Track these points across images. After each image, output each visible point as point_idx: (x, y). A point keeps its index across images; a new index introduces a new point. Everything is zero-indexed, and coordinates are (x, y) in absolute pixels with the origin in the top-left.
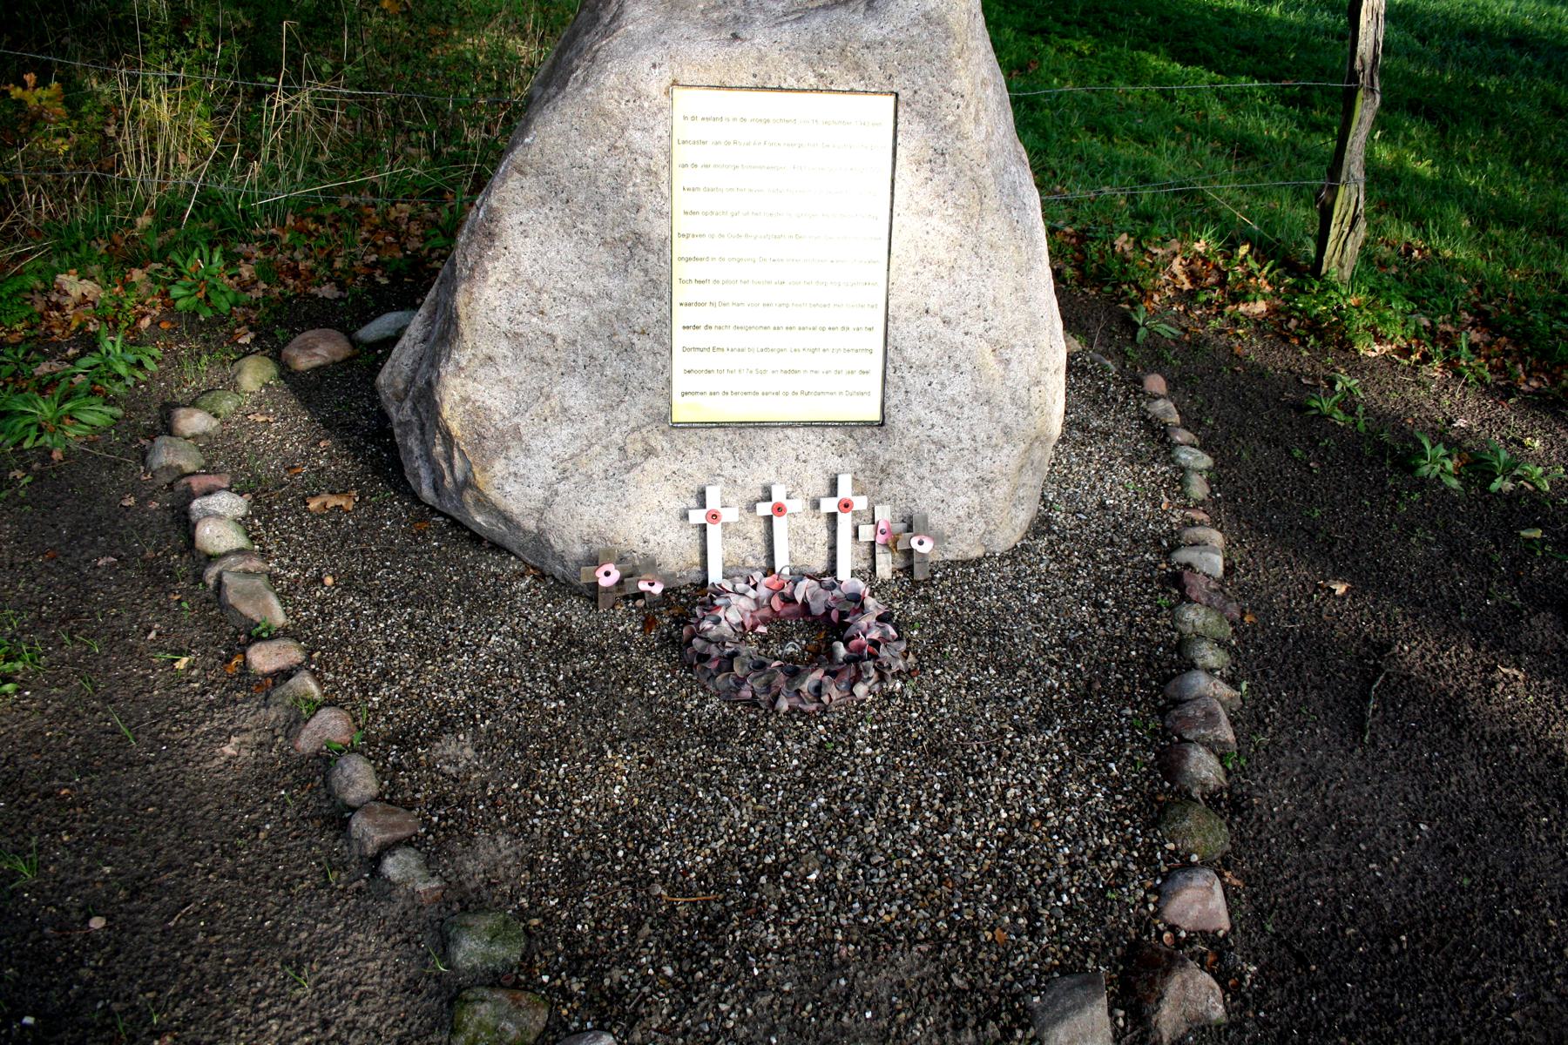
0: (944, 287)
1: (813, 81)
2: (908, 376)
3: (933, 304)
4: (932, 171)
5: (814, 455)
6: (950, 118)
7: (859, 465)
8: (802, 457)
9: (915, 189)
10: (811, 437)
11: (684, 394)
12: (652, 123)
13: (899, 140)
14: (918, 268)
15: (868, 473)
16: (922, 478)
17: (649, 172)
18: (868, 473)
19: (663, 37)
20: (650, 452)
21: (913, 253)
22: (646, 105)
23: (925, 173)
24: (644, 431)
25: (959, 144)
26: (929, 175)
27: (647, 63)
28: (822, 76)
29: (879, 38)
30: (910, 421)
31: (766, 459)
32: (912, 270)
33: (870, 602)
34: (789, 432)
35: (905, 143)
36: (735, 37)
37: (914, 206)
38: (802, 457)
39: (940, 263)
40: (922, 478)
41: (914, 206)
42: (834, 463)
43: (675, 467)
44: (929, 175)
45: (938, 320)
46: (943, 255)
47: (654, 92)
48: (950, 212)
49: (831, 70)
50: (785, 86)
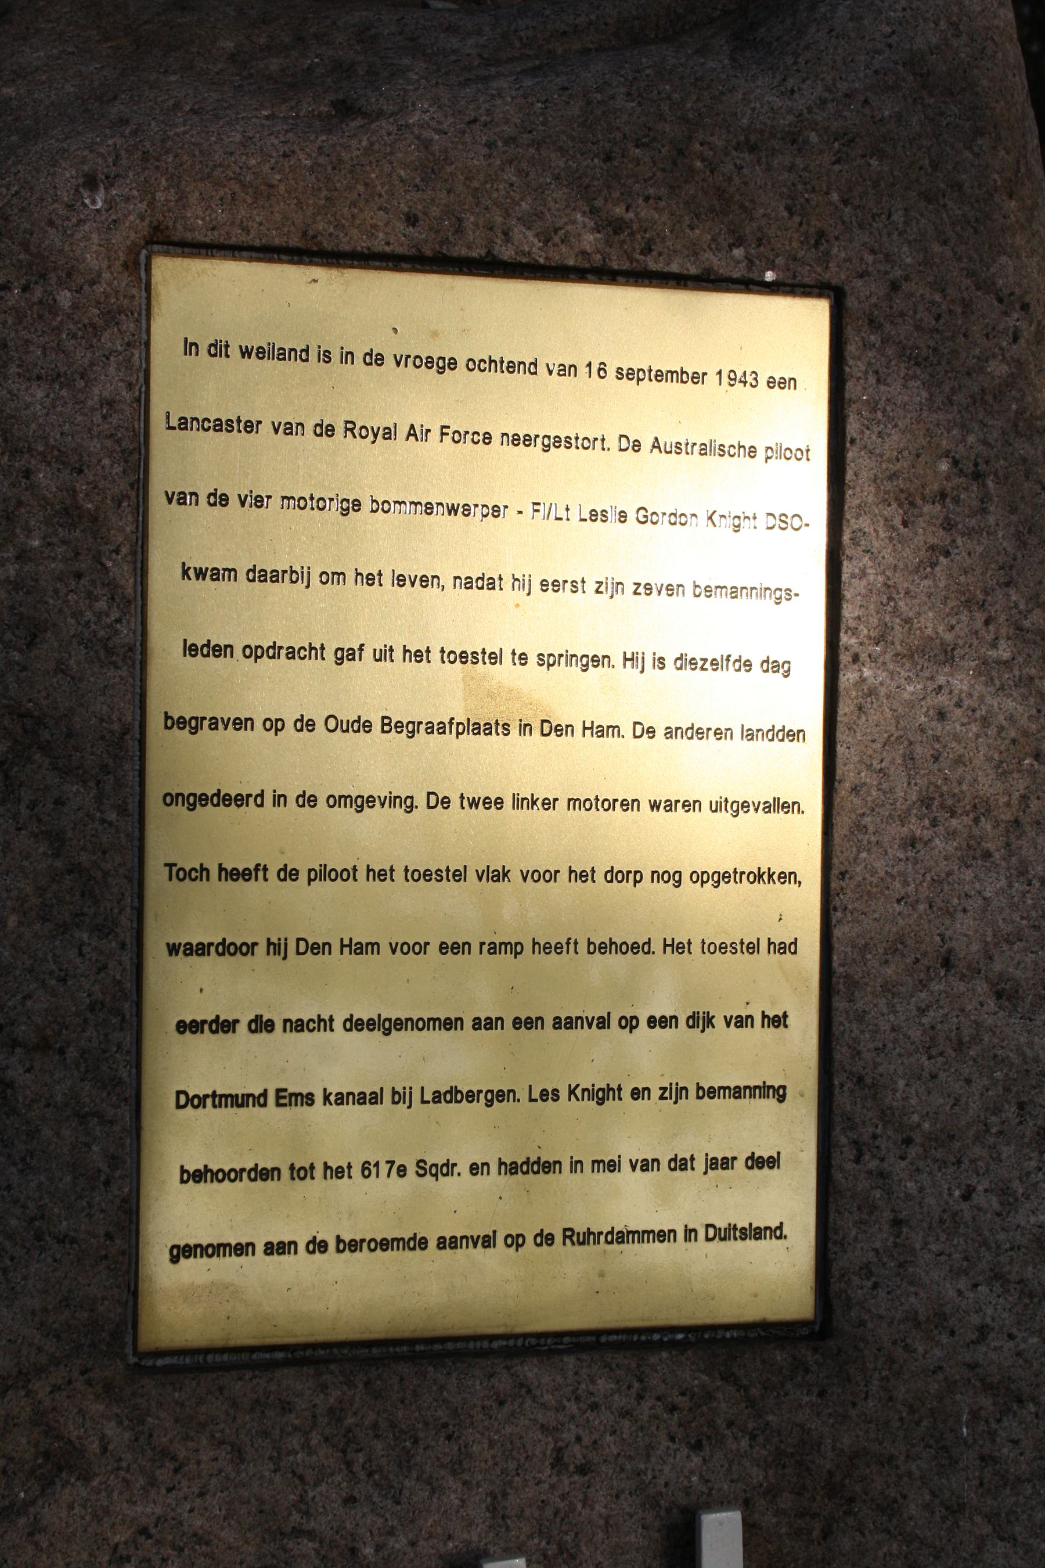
0: (992, 885)
1: (589, 240)
2: (900, 1168)
3: (966, 932)
4: (948, 525)
5: (611, 1445)
6: (998, 368)
7: (757, 1474)
8: (576, 1454)
9: (901, 581)
10: (603, 1385)
11: (180, 1253)
12: (82, 357)
13: (853, 427)
14: (916, 827)
15: (786, 1501)
16: (956, 1509)
17: (70, 513)
18: (786, 1501)
19: (115, 110)
20: (61, 1462)
21: (899, 779)
22: (65, 298)
23: (926, 534)
24: (41, 1388)
25: (1023, 448)
26: (939, 537)
27: (68, 175)
28: (617, 226)
29: (786, 121)
30: (912, 1318)
31: (456, 1468)
32: (895, 830)
33: (911, 674)
34: (530, 1370)
35: (871, 438)
36: (345, 109)
37: (898, 632)
38: (576, 1454)
39: (981, 808)
40: (956, 1509)
41: (898, 632)
42: (678, 1468)
43: (145, 1511)
44: (939, 537)
45: (982, 987)
46: (987, 784)
47: (92, 260)
48: (1004, 652)
49: (645, 212)
50: (506, 253)
